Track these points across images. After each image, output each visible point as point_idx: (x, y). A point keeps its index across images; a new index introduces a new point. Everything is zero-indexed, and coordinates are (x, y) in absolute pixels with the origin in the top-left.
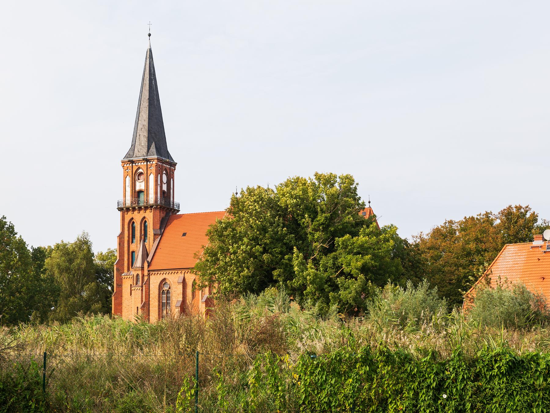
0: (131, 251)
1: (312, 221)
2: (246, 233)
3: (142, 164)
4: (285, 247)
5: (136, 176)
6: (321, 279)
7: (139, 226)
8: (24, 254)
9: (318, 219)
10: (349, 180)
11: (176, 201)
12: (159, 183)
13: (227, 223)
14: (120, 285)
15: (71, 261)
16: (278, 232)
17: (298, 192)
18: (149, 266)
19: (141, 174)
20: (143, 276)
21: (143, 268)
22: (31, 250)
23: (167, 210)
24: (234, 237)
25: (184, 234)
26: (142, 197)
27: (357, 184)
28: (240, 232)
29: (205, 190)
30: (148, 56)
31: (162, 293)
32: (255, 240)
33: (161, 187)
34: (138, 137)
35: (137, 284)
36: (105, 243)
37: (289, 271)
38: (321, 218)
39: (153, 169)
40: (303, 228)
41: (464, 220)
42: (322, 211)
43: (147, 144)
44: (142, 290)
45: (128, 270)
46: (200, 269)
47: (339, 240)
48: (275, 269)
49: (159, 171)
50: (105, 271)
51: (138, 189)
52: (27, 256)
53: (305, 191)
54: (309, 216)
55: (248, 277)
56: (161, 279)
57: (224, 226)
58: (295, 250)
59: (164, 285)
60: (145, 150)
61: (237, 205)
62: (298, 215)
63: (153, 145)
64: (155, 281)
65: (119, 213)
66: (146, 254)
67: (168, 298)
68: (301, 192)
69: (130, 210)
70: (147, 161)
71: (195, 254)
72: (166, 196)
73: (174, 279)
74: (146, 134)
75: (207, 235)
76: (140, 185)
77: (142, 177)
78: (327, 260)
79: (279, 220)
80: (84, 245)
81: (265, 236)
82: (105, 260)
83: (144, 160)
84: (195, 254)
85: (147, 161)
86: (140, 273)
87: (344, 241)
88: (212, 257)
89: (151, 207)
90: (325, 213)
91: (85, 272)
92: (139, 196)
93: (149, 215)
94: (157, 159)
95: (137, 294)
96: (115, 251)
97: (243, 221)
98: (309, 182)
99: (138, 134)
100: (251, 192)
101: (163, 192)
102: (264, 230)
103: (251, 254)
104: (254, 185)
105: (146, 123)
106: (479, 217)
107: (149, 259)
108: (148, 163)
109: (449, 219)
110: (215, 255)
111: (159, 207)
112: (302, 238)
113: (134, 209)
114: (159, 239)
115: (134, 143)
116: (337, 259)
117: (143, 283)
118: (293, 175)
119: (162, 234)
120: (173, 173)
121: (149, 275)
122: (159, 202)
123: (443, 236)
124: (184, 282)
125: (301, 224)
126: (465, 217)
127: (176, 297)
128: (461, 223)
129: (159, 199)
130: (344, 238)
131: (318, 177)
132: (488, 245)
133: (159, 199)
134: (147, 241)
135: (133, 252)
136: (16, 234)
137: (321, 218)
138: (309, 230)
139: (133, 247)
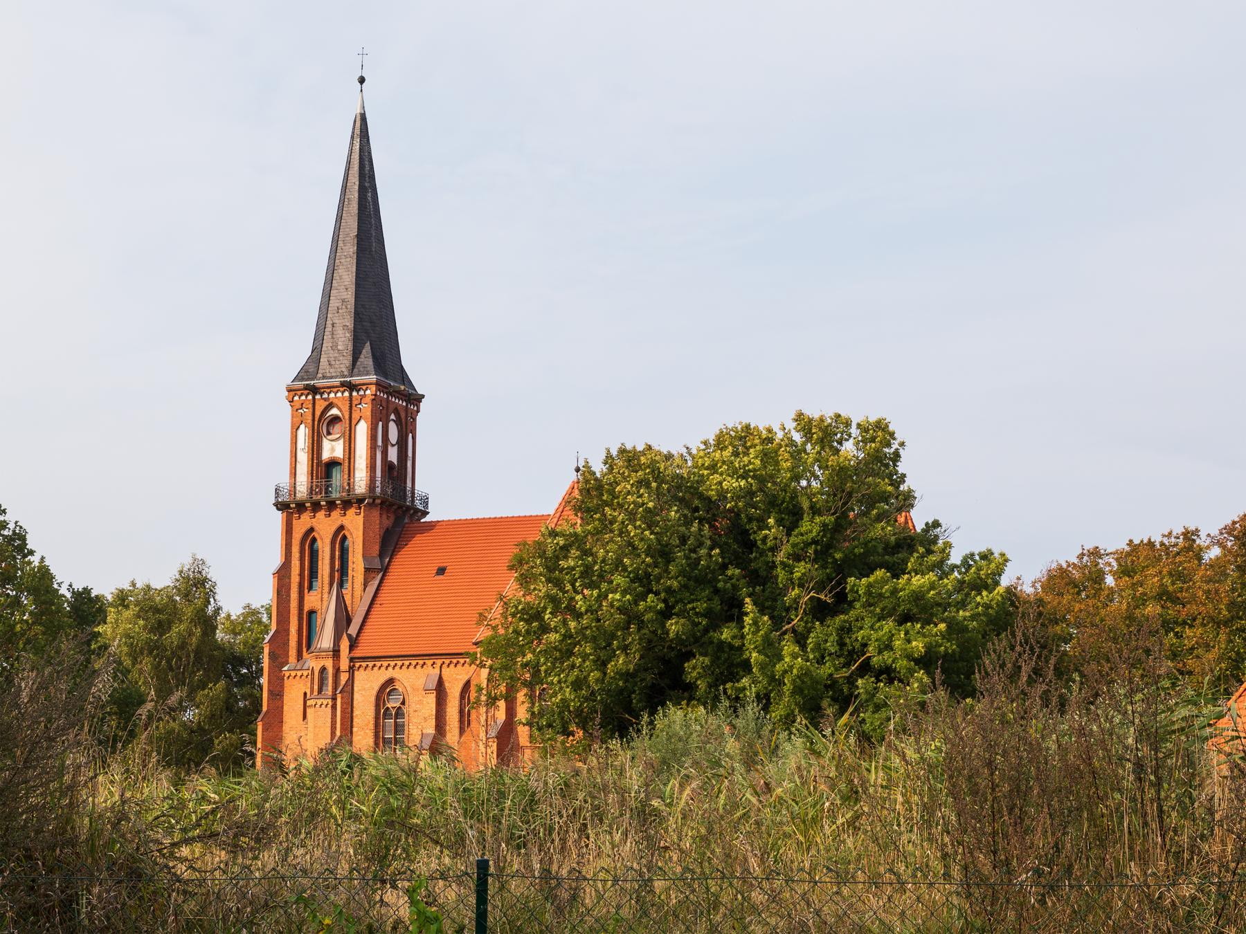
0: (306, 609)
1: (789, 535)
2: (618, 565)
3: (339, 394)
4: (717, 600)
5: (323, 424)
6: (815, 682)
7: (327, 550)
8: (53, 604)
9: (803, 529)
10: (878, 433)
11: (421, 487)
12: (380, 443)
13: (571, 535)
14: (277, 694)
15: (161, 627)
16: (699, 559)
17: (753, 460)
18: (352, 648)
19: (335, 420)
20: (337, 671)
21: (336, 653)
22: (69, 595)
23: (396, 511)
24: (587, 571)
25: (441, 571)
26: (338, 478)
27: (902, 444)
28: (603, 561)
29: (497, 461)
30: (358, 131)
31: (385, 714)
32: (643, 582)
33: (385, 453)
34: (329, 329)
35: (320, 691)
36: (245, 586)
37: (726, 660)
38: (810, 527)
39: (366, 408)
40: (762, 553)
41: (1127, 549)
42: (815, 511)
43: (350, 347)
44: (334, 707)
45: (300, 656)
46: (500, 651)
47: (858, 584)
48: (689, 655)
49: (380, 415)
50: (238, 661)
51: (326, 455)
52: (60, 609)
53: (769, 457)
54: (779, 522)
55: (626, 676)
56: (382, 680)
57: (562, 543)
58: (749, 606)
59: (389, 694)
60: (347, 361)
61: (592, 494)
62: (750, 520)
63: (367, 350)
64: (367, 684)
65: (278, 517)
66: (343, 618)
67: (398, 729)
68: (758, 462)
69: (306, 509)
70: (351, 387)
71: (481, 614)
72: (397, 472)
73: (414, 682)
74: (349, 322)
75: (511, 568)
76: (333, 449)
77: (337, 428)
78: (823, 634)
79: (700, 530)
80: (196, 585)
81: (667, 571)
82: (236, 634)
83: (343, 384)
84: (481, 614)
85: (351, 387)
86: (329, 664)
87: (870, 585)
88: (528, 622)
89: (360, 501)
90: (820, 515)
91: (197, 652)
92: (328, 475)
93: (354, 522)
94: (377, 384)
95: (321, 716)
96: (262, 610)
97: (612, 531)
98: (780, 435)
99: (329, 323)
100: (630, 458)
101: (388, 466)
102: (663, 554)
103: (631, 616)
104: (637, 443)
105: (350, 296)
106: (1166, 541)
107: (353, 630)
108: (355, 394)
109: (1089, 546)
110: (538, 616)
111: (378, 501)
112: (747, 578)
113: (316, 507)
114: (377, 582)
115: (318, 344)
116: (850, 630)
117: (335, 689)
118: (734, 420)
119: (385, 570)
120: (415, 420)
121: (351, 670)
122: (378, 490)
123: (1076, 586)
124: (440, 690)
125: (759, 543)
126: (1131, 541)
127: (419, 724)
128: (1120, 556)
129: (378, 484)
130: (872, 579)
131: (805, 424)
132: (1192, 609)
133: (378, 484)
134: (348, 585)
135: (312, 612)
136: (31, 553)
137: (810, 527)
138: (781, 557)
139: (311, 600)
